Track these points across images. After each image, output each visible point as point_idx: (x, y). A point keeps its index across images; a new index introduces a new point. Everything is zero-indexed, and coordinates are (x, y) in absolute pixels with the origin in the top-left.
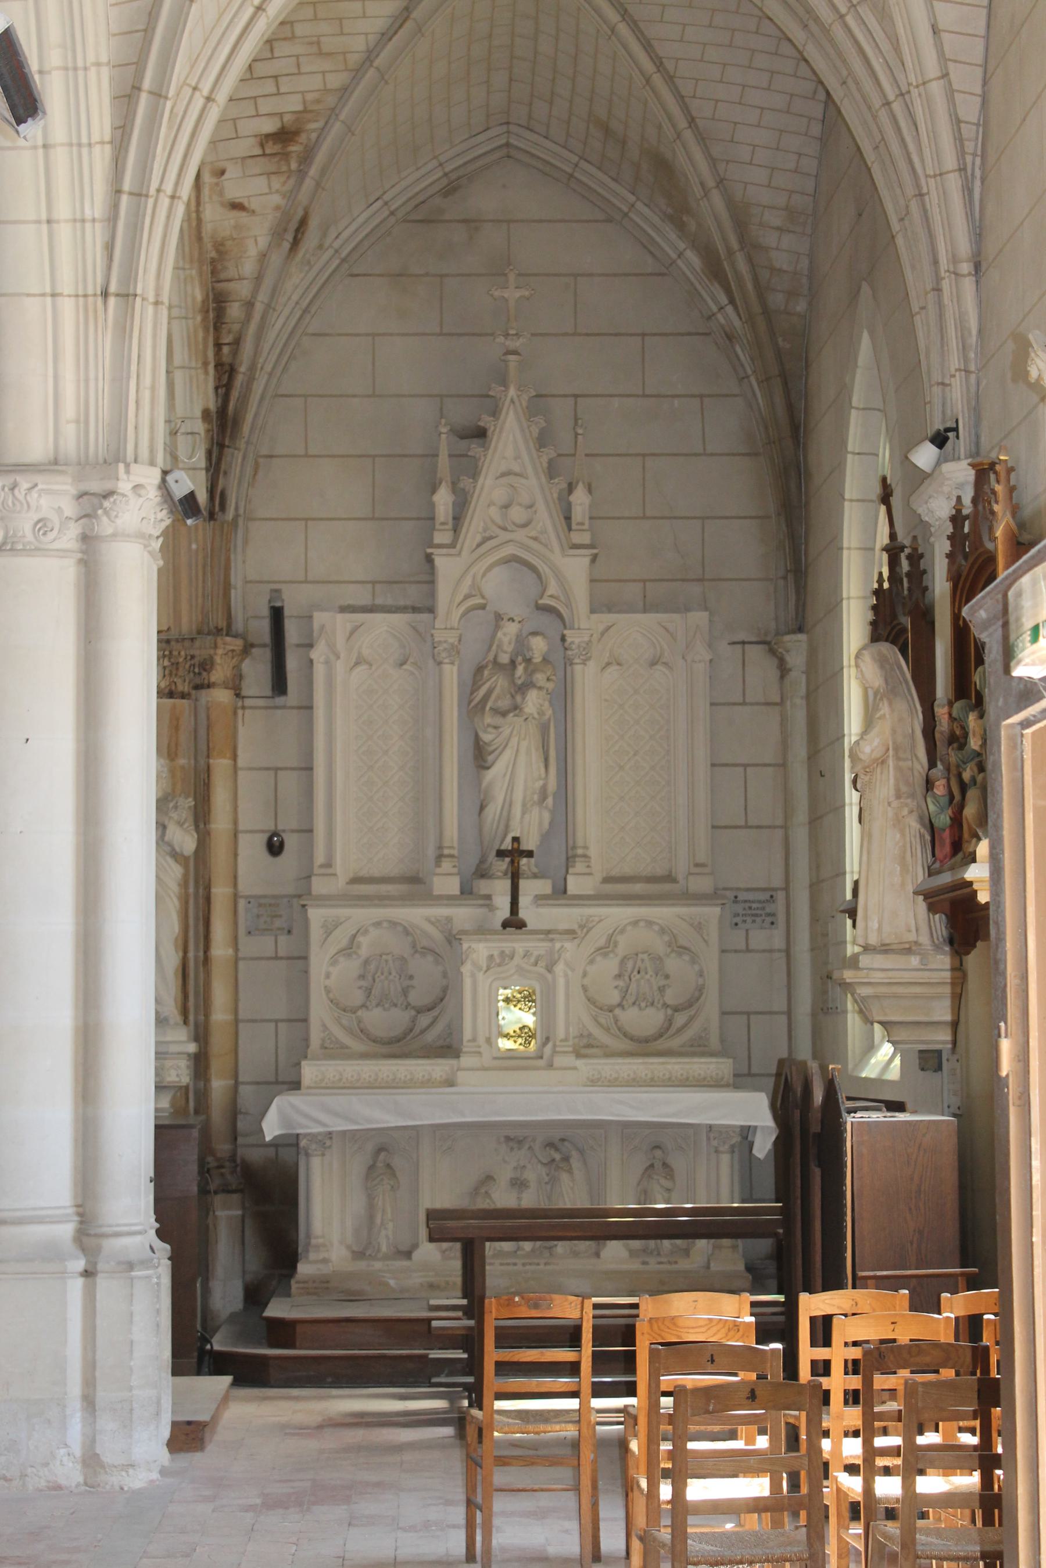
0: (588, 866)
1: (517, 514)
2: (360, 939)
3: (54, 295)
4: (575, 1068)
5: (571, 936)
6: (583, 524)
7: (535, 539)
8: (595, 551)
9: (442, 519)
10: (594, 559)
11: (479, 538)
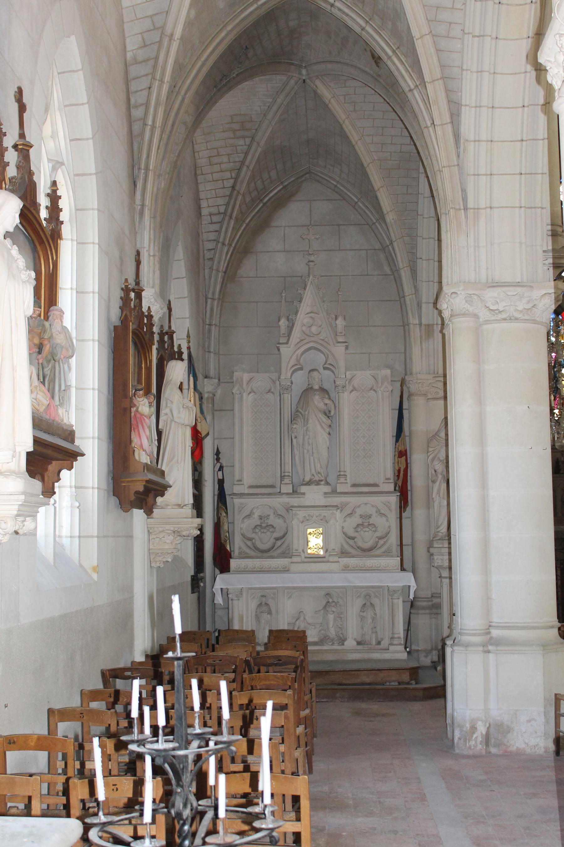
0: (346, 480)
1: (314, 329)
2: (255, 511)
3: (491, 208)
4: (338, 562)
5: (336, 508)
6: (342, 333)
7: (323, 340)
8: (347, 344)
9: (283, 332)
10: (347, 348)
11: (298, 340)
